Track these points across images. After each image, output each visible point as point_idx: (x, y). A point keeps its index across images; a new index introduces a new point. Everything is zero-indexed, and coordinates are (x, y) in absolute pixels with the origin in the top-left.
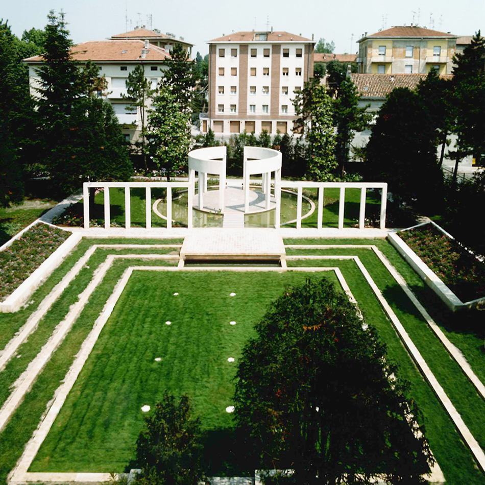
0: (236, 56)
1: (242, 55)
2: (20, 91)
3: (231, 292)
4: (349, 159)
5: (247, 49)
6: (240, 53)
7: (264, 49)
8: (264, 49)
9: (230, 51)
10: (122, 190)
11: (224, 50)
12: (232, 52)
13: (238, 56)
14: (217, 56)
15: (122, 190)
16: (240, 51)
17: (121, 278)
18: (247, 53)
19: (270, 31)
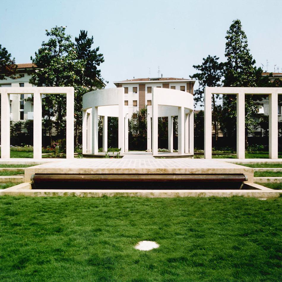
0: (136, 92)
1: (141, 92)
2: (280, 101)
3: (140, 238)
4: (133, 136)
5: (145, 88)
6: (139, 90)
7: (133, 88)
8: (133, 88)
9: (132, 89)
10: (234, 97)
11: (128, 88)
12: (133, 89)
13: (138, 92)
14: (146, 92)
15: (234, 97)
16: (139, 88)
17: (214, 196)
18: (145, 90)
19: (161, 77)
